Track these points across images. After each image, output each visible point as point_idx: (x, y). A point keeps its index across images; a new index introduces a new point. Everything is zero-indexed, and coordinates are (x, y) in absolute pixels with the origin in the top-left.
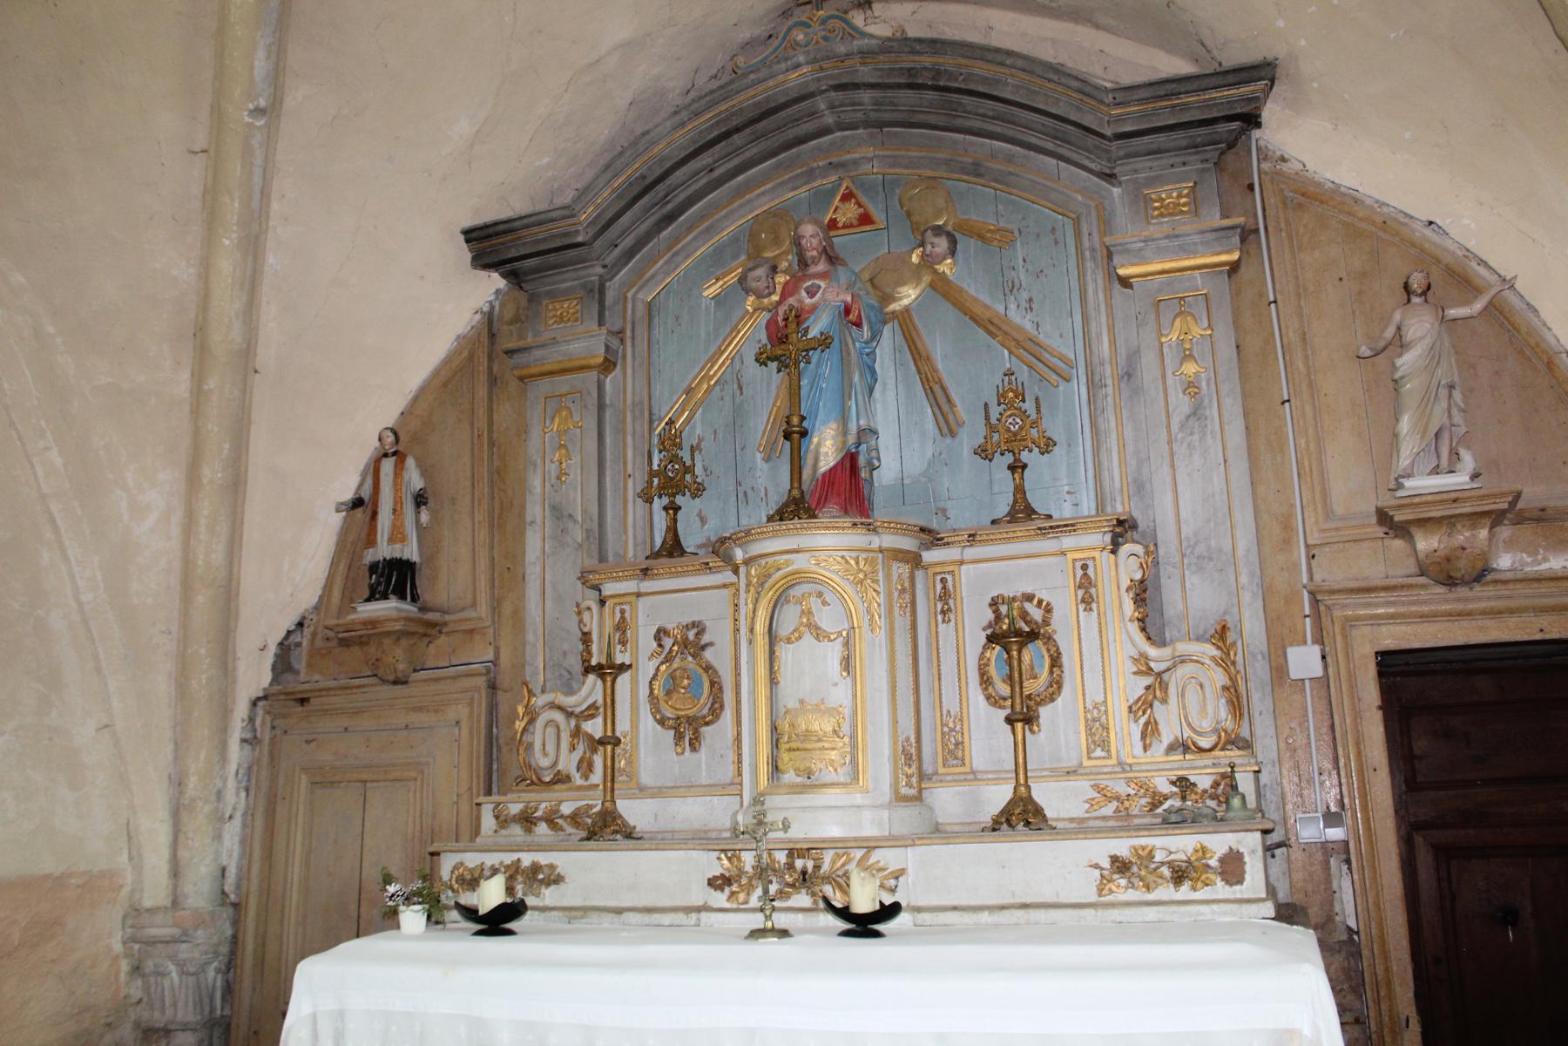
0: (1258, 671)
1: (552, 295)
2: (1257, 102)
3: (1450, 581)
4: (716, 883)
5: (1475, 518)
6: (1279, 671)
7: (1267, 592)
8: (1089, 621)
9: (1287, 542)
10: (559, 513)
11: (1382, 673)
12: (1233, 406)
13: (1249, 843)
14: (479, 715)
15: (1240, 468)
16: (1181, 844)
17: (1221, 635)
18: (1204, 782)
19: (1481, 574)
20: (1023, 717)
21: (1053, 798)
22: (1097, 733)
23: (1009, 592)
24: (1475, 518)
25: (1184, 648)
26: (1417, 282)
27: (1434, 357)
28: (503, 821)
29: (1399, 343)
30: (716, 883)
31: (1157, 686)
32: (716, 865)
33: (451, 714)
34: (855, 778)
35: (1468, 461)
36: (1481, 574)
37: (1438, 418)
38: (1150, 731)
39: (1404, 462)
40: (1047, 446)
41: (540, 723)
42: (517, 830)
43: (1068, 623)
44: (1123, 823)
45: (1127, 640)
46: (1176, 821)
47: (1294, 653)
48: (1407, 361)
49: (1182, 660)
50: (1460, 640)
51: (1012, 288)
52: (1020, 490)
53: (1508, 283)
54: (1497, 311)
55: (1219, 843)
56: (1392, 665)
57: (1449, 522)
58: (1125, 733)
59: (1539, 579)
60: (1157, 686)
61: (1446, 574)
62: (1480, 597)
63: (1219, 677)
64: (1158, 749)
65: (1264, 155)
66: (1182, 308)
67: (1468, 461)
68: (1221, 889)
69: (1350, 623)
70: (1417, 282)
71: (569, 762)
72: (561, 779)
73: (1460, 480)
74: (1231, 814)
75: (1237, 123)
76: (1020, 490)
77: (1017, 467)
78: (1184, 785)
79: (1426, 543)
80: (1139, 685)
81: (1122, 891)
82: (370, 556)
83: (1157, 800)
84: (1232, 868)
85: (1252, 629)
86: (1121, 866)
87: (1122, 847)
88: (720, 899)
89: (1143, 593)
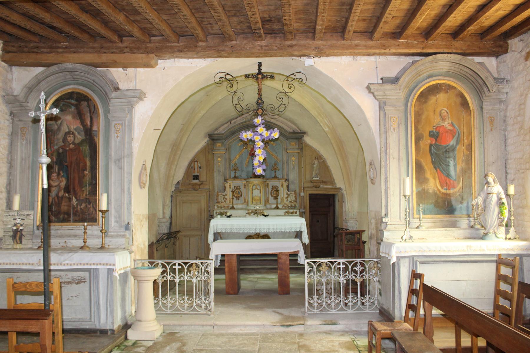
0: (298, 195)
1: (218, 143)
2: (303, 136)
3: (316, 187)
4: (247, 213)
5: (319, 182)
6: (300, 195)
7: (299, 187)
8: (282, 189)
9: (301, 182)
10: (219, 171)
11: (309, 197)
12: (297, 167)
13: (298, 211)
14: (413, 207)
15: (298, 174)
16: (292, 211)
17: (295, 191)
18: (293, 205)
19: (319, 187)
20: (276, 198)
21: (280, 206)
22: (282, 200)
23: (274, 185)
24: (319, 182)
25: (291, 192)
26: (317, 157)
27: (317, 166)
28: (218, 207)
29: (314, 164)
30: (247, 213)
31: (288, 196)
32: (247, 212)
33: (203, 194)
34: (261, 203)
35: (319, 176)
36: (319, 187)
37: (317, 172)
38: (287, 200)
39: (313, 176)
40: (279, 170)
41: (219, 197)
42: (219, 208)
43: (280, 189)
44: (285, 208)
45: (286, 191)
46: (291, 209)
47: (301, 193)
48: (315, 166)
49: (291, 193)
50: (518, 17)
51: (275, 151)
52: (275, 175)
53: (325, 159)
54: (323, 161)
55: (295, 210)
56: (309, 194)
57: (317, 182)
58: (285, 200)
59: (324, 188)
60: (288, 196)
61: (316, 187)
62: (319, 189)
63: (294, 195)
64: (288, 202)
65: (303, 140)
66: (293, 156)
67: (319, 176)
68: (295, 214)
69: (307, 191)
70: (317, 157)
71: (223, 201)
72: (222, 203)
73: (318, 179)
74: (491, 94)
75: (319, 347)
76: (275, 175)
77: (275, 172)
78: (291, 206)
79: (314, 184)
80: (287, 196)
81: (287, 214)
82: (194, 174)
83: (289, 207)
84: (296, 213)
85: (297, 191)
86: (286, 212)
87: (287, 211)
88: (247, 215)
89: (288, 187)
